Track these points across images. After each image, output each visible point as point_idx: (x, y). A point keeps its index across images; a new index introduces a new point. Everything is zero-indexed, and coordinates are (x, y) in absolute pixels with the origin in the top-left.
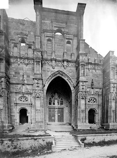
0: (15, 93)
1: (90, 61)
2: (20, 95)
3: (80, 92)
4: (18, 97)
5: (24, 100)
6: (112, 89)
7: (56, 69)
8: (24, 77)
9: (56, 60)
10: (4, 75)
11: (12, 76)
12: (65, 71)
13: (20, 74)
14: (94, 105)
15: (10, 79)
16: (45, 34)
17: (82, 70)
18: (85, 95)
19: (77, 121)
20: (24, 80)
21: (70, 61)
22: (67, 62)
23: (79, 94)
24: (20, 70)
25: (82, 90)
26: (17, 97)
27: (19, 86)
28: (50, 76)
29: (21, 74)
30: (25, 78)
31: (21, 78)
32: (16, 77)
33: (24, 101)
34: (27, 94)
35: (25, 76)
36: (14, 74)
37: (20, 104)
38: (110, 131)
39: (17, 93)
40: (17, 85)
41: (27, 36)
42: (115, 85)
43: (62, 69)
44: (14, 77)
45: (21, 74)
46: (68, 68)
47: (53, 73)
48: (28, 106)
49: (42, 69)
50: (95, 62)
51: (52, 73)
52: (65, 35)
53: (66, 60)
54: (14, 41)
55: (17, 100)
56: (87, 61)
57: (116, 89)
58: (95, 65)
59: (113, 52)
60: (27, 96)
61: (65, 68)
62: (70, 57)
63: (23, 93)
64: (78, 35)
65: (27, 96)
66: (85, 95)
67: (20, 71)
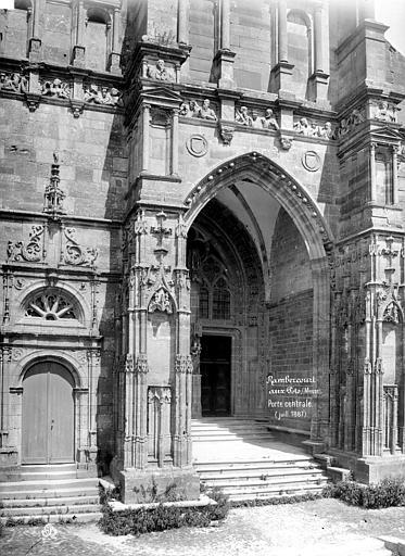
1: (228, 79)
2: (34, 285)
3: (379, 290)
4: (18, 297)
5: (53, 312)
6: (382, 262)
7: (241, 145)
8: (61, 176)
12: (281, 160)
14: (173, 411)
21: (308, 110)
22: (294, 113)
23: (370, 296)
24: (40, 135)
25: (153, 261)
26: (16, 293)
27: (29, 228)
30: (62, 186)
33: (50, 317)
35: (66, 174)
37: (30, 336)
40: (13, 225)
42: (396, 246)
43: (266, 148)
46: (299, 148)
47: (221, 162)
48: (79, 349)
50: (274, 86)
55: (13, 312)
56: (265, 83)
57: (402, 265)
61: (285, 145)
62: (303, 87)
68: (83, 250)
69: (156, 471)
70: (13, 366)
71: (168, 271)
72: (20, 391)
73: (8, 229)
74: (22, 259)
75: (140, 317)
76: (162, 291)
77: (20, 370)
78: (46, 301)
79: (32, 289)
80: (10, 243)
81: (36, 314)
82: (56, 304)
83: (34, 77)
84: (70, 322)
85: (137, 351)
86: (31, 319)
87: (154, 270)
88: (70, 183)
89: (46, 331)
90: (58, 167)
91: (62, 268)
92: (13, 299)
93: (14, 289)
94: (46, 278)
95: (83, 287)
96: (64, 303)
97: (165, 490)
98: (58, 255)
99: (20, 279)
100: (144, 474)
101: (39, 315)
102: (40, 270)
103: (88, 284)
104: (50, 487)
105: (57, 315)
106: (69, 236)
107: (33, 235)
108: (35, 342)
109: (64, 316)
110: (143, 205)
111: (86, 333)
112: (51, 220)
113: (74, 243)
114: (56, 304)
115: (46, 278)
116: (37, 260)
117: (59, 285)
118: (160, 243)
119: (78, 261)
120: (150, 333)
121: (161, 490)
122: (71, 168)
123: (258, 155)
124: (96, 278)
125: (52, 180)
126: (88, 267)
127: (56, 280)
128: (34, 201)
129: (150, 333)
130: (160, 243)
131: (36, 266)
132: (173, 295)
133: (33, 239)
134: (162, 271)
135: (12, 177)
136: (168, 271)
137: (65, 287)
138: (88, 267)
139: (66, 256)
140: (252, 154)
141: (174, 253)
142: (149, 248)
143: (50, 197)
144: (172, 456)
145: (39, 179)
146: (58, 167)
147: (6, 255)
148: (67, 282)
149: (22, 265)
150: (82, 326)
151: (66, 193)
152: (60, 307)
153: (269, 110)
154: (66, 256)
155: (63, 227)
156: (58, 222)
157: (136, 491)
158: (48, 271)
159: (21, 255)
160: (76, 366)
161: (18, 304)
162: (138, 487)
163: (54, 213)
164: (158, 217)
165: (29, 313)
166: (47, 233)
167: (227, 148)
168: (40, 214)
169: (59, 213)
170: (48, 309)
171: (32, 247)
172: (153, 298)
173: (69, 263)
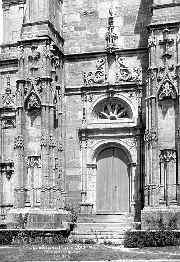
0: (82, 89)
2: (99, 98)
4: (90, 106)
5: (114, 115)
8: (115, 24)
9: (82, 243)
10: (46, 31)
11: (73, 29)
13: (100, 16)
15: (63, 41)
20: (115, 38)
25: (160, 64)
26: (89, 104)
27: (95, 63)
30: (116, 31)
31: (103, 32)
32: (84, 29)
33: (113, 118)
34: (126, 88)
37: (98, 131)
38: (78, 88)
39: (87, 89)
44: (79, 32)
45: (104, 15)
48: (129, 136)
55: (88, 117)
60: (124, 96)
63: (110, 90)
64: (136, 127)
65: (124, 96)
68: (131, 70)
69: (163, 209)
70: (89, 151)
71: (172, 69)
72: (94, 167)
73: (83, 65)
74: (92, 83)
75: (151, 102)
76: (167, 84)
77: (93, 152)
78: (109, 108)
79: (98, 101)
80: (85, 73)
81: (104, 117)
82: (116, 110)
84: (126, 120)
85: (150, 126)
86: (101, 121)
87: (162, 70)
88: (121, 28)
89: (108, 126)
90: (112, 19)
91: (117, 84)
92: (88, 108)
93: (88, 102)
94: (107, 92)
95: (131, 95)
96: (121, 108)
97: (169, 222)
98: (115, 77)
99: (91, 96)
100: (155, 210)
101: (107, 118)
102: (103, 88)
103: (134, 92)
104: (108, 226)
105: (116, 116)
106: (121, 62)
107: (99, 66)
108: (101, 135)
109: (122, 116)
110: (152, 26)
112: (108, 53)
113: (124, 67)
114: (116, 110)
115: (107, 92)
116: (102, 82)
117: (116, 96)
118: (165, 50)
119: (128, 77)
120: (160, 115)
121: (166, 221)
122: (121, 18)
124: (139, 87)
125: (109, 28)
126: (134, 81)
127: (113, 93)
128: (99, 44)
129: (160, 115)
130: (165, 50)
131: (101, 85)
132: (174, 85)
133: (98, 69)
134: (167, 69)
135: (84, 32)
136: (172, 69)
137: (120, 97)
138: (134, 81)
139: (120, 76)
141: (176, 56)
142: (158, 56)
143: (107, 39)
144: (177, 199)
145: (101, 30)
146: (112, 19)
147: (83, 81)
148: (120, 93)
149: (92, 86)
150: (131, 121)
151: (119, 35)
152: (118, 112)
154: (120, 76)
155: (117, 57)
156: (113, 54)
157: (149, 221)
158: (107, 87)
159: (92, 80)
160: (128, 148)
161: (91, 111)
162: (150, 219)
163: (109, 48)
164: (164, 33)
165: (100, 117)
166: (107, 63)
168: (103, 51)
169: (112, 48)
170: (111, 113)
171: (98, 74)
172: (161, 89)
173: (121, 80)
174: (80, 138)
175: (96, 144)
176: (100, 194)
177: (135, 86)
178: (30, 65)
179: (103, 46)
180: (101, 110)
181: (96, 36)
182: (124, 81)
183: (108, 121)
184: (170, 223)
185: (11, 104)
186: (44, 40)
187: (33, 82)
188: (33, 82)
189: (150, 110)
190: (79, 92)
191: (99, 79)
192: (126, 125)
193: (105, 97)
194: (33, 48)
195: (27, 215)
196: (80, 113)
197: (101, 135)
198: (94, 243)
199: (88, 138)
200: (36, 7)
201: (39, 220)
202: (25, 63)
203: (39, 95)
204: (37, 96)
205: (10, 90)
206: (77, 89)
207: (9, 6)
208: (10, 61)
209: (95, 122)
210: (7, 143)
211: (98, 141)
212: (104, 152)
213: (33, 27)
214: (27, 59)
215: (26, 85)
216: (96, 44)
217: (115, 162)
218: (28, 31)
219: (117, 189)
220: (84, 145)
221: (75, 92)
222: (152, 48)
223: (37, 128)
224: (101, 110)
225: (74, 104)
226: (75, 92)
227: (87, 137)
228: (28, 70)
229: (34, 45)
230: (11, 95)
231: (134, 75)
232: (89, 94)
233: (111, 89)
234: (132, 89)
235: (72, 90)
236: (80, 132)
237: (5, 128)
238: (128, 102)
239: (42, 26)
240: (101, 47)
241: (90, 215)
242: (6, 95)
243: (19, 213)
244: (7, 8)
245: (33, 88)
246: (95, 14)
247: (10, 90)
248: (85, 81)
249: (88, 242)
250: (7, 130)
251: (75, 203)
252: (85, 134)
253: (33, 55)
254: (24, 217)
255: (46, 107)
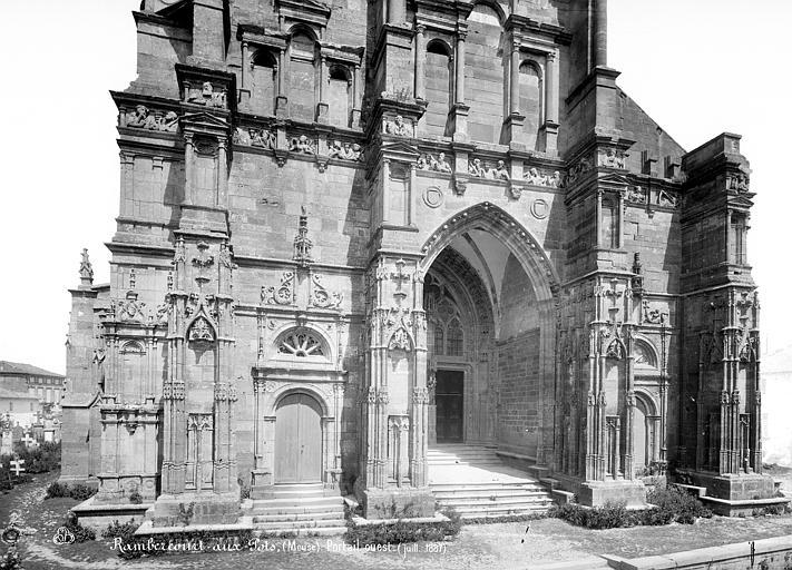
0: (259, 310)
2: (286, 325)
4: (270, 336)
5: (303, 349)
6: (606, 303)
7: (474, 196)
8: (308, 226)
11: (245, 219)
12: (511, 209)
13: (288, 211)
16: (422, 19)
17: (605, 218)
18: (410, 330)
19: (584, 463)
26: (269, 333)
27: (279, 274)
28: (442, 229)
29: (293, 210)
30: (309, 236)
31: (292, 235)
32: (263, 223)
33: (301, 354)
35: (313, 225)
36: (255, 209)
37: (283, 371)
39: (267, 311)
41: (328, 15)
43: (497, 198)
45: (293, 210)
48: (326, 382)
49: (229, 168)
51: (450, 216)
52: (516, 32)
53: (525, 154)
54: (259, 39)
55: (266, 349)
58: (649, 186)
59: (737, 138)
61: (515, 195)
66: (410, 330)
67: (287, 196)
68: (330, 294)
72: (273, 419)
76: (401, 331)
78: (296, 340)
83: (281, 134)
84: (318, 358)
89: (296, 366)
99: (273, 320)
100: (385, 493)
101: (291, 353)
105: (306, 352)
106: (317, 281)
108: (286, 376)
111: (332, 368)
112: (300, 267)
117: (308, 325)
118: (399, 287)
120: (390, 369)
121: (400, 507)
123: (489, 205)
126: (334, 309)
127: (305, 321)
129: (390, 369)
130: (399, 287)
137: (314, 327)
138: (334, 309)
139: (314, 299)
140: (484, 204)
141: (412, 296)
149: (275, 308)
151: (314, 242)
153: (500, 162)
158: (298, 313)
160: (324, 397)
166: (296, 279)
167: (461, 199)
168: (290, 261)
173: (317, 306)
174: (256, 380)
175: (279, 388)
176: (279, 458)
177: (336, 316)
178: (196, 272)
179: (292, 254)
180: (286, 341)
181: (281, 238)
182: (321, 307)
183: (293, 357)
184: (405, 510)
185: (138, 317)
186: (222, 239)
187: (202, 301)
188: (202, 301)
189: (379, 363)
190: (255, 313)
191: (283, 300)
192: (322, 368)
193: (291, 326)
194: (201, 247)
195: (192, 504)
196: (255, 345)
197: (286, 376)
198: (294, 537)
199: (267, 379)
200: (201, 181)
201: (213, 512)
202: (187, 268)
203: (212, 322)
204: (208, 323)
205: (137, 295)
206: (251, 309)
207: (134, 157)
208: (135, 248)
209: (274, 358)
210: (127, 377)
211: (282, 384)
212: (289, 397)
213: (199, 212)
214: (190, 262)
215: (189, 302)
216: (281, 249)
217: (302, 411)
218: (190, 217)
219: (304, 449)
220: (261, 390)
221: (247, 313)
222: (134, 113)
223: (205, 369)
224: (286, 341)
225: (245, 329)
226: (247, 313)
227: (267, 379)
228: (191, 280)
229: (203, 243)
230: (137, 303)
231: (334, 301)
232: (270, 317)
233: (303, 316)
234: (332, 319)
235: (244, 308)
236: (255, 371)
237: (124, 353)
238: (325, 336)
239: (216, 214)
240: (289, 255)
241: (268, 488)
242: (127, 302)
243: (178, 502)
244: (130, 160)
245: (202, 308)
246: (279, 205)
247: (137, 295)
248: (263, 298)
249: (284, 536)
250: (126, 356)
251: (245, 469)
252: (259, 375)
253: (204, 260)
254: (186, 509)
255: (225, 341)
